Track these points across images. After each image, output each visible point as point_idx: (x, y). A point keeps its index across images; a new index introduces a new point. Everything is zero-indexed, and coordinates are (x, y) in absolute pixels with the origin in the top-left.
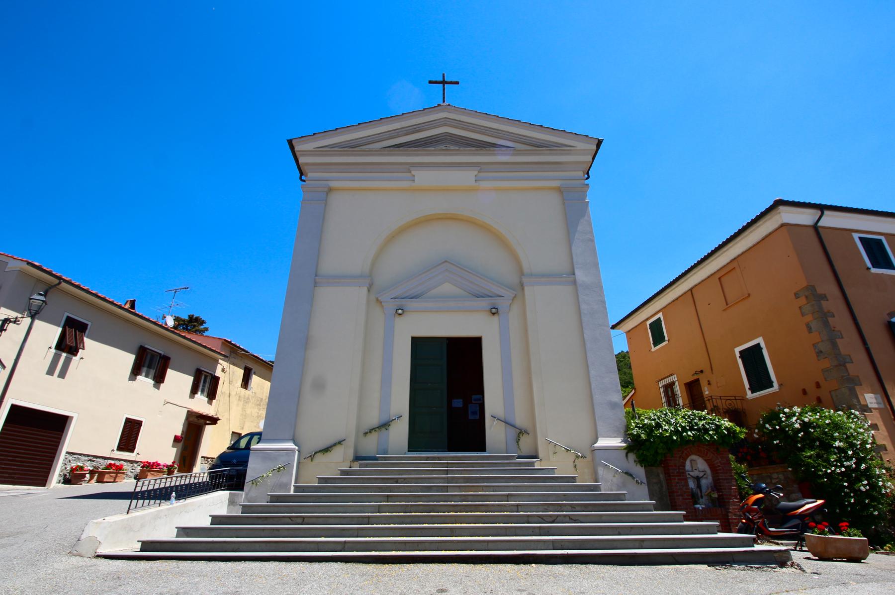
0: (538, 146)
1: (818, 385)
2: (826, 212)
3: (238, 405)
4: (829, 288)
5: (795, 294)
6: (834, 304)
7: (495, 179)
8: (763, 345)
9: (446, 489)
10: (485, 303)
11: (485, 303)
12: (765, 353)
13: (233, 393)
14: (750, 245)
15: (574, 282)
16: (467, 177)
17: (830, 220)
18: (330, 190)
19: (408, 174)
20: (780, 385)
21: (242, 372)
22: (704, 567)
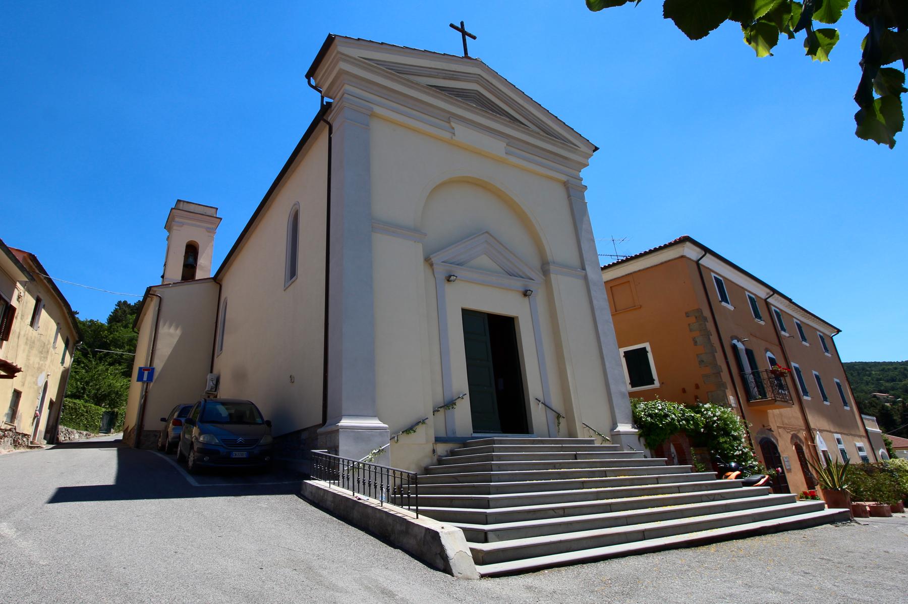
0: (549, 134)
1: (697, 387)
2: (708, 255)
3: (24, 350)
4: (707, 313)
5: (686, 313)
6: (710, 326)
7: (524, 159)
8: (649, 349)
9: (605, 474)
10: (519, 284)
11: (519, 284)
12: (650, 356)
13: (22, 333)
14: (648, 266)
15: (586, 278)
16: (498, 147)
17: (708, 262)
18: (373, 115)
19: (447, 125)
20: (662, 383)
21: (34, 302)
22: (829, 525)
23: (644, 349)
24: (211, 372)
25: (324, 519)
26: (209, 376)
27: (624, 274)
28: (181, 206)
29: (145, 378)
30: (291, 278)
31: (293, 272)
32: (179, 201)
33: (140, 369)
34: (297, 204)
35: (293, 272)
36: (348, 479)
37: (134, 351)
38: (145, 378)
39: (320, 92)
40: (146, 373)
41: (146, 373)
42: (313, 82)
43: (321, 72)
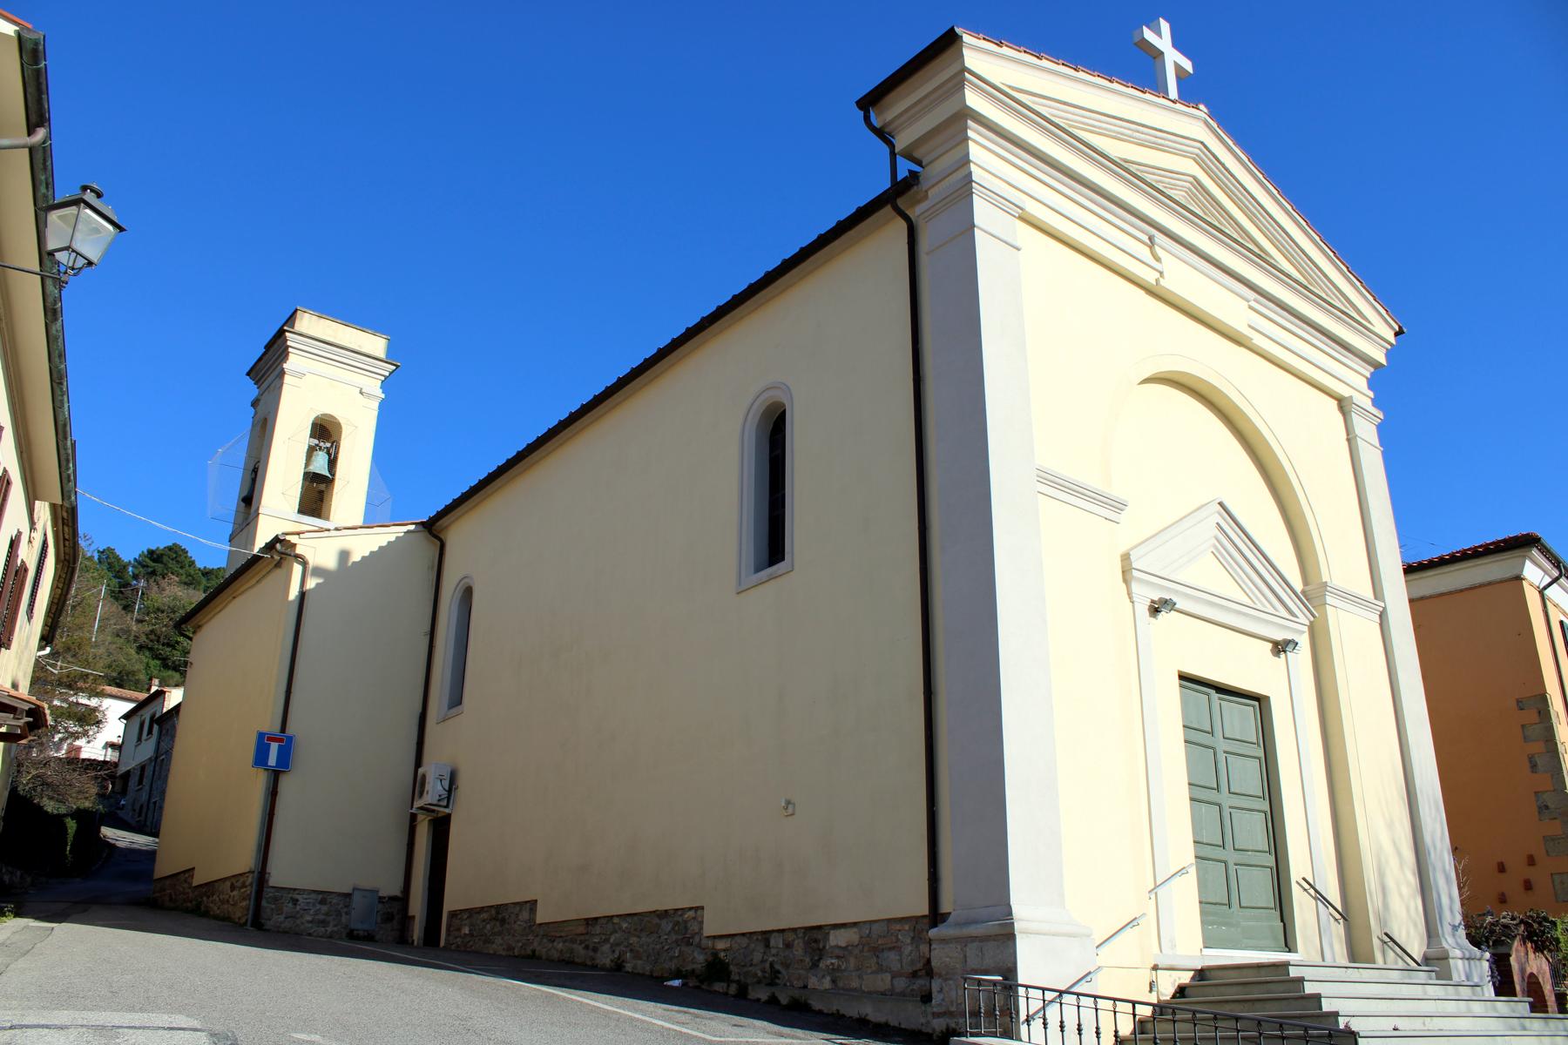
5: (1518, 701)
29: (272, 761)
33: (261, 735)
38: (272, 761)
40: (274, 747)
41: (274, 747)
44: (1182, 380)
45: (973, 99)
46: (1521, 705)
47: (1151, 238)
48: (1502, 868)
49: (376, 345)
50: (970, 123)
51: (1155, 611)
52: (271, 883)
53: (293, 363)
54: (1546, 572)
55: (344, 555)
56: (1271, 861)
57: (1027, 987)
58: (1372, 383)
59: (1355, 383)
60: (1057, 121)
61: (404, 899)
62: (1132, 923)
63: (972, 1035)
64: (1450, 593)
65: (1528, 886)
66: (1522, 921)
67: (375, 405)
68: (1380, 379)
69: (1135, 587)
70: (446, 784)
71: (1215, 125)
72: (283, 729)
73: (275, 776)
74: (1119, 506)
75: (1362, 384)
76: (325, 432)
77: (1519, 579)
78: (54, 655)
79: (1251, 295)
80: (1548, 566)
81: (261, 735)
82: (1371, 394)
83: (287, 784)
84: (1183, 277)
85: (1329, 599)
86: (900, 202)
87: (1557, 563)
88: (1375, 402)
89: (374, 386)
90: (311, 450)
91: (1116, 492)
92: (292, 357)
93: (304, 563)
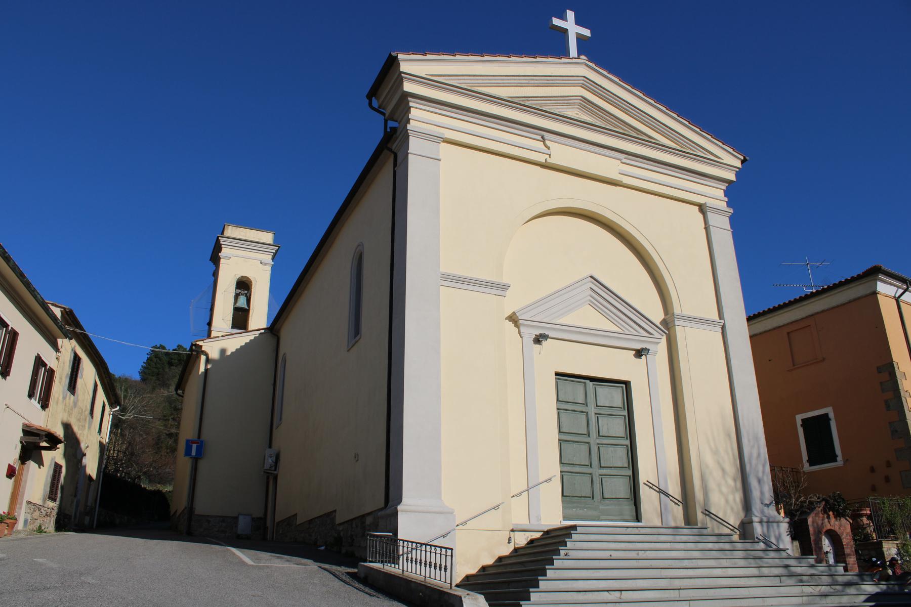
5: (878, 368)
20: (846, 461)
23: (826, 415)
24: (270, 447)
25: (729, 436)
26: (268, 452)
27: (804, 315)
28: (449, 552)
29: (194, 453)
30: (355, 336)
31: (356, 330)
32: (452, 549)
33: (188, 441)
34: (361, 245)
35: (356, 330)
36: (446, 569)
37: (178, 427)
38: (194, 453)
39: (384, 114)
40: (194, 446)
41: (194, 446)
42: (375, 103)
43: (384, 92)
44: (582, 213)
45: (408, 87)
46: (879, 370)
47: (542, 137)
48: (872, 470)
49: (267, 237)
50: (410, 99)
51: (538, 340)
52: (196, 513)
53: (225, 252)
54: (898, 287)
55: (223, 351)
56: (630, 473)
57: (404, 541)
58: (726, 193)
59: (716, 196)
60: (463, 86)
61: (264, 519)
62: (496, 508)
63: (370, 562)
64: (838, 306)
65: (887, 479)
66: (823, 499)
67: (269, 268)
68: (732, 191)
69: (522, 329)
70: (274, 459)
71: (593, 65)
72: (199, 437)
73: (196, 461)
74: (505, 287)
75: (721, 194)
76: (244, 285)
77: (875, 293)
78: (123, 410)
79: (622, 156)
80: (899, 284)
81: (188, 441)
82: (726, 199)
83: (203, 465)
84: (562, 153)
85: (677, 322)
86: (389, 145)
87: (903, 280)
88: (729, 204)
89: (268, 258)
90: (237, 296)
91: (505, 281)
92: (224, 249)
93: (206, 355)
